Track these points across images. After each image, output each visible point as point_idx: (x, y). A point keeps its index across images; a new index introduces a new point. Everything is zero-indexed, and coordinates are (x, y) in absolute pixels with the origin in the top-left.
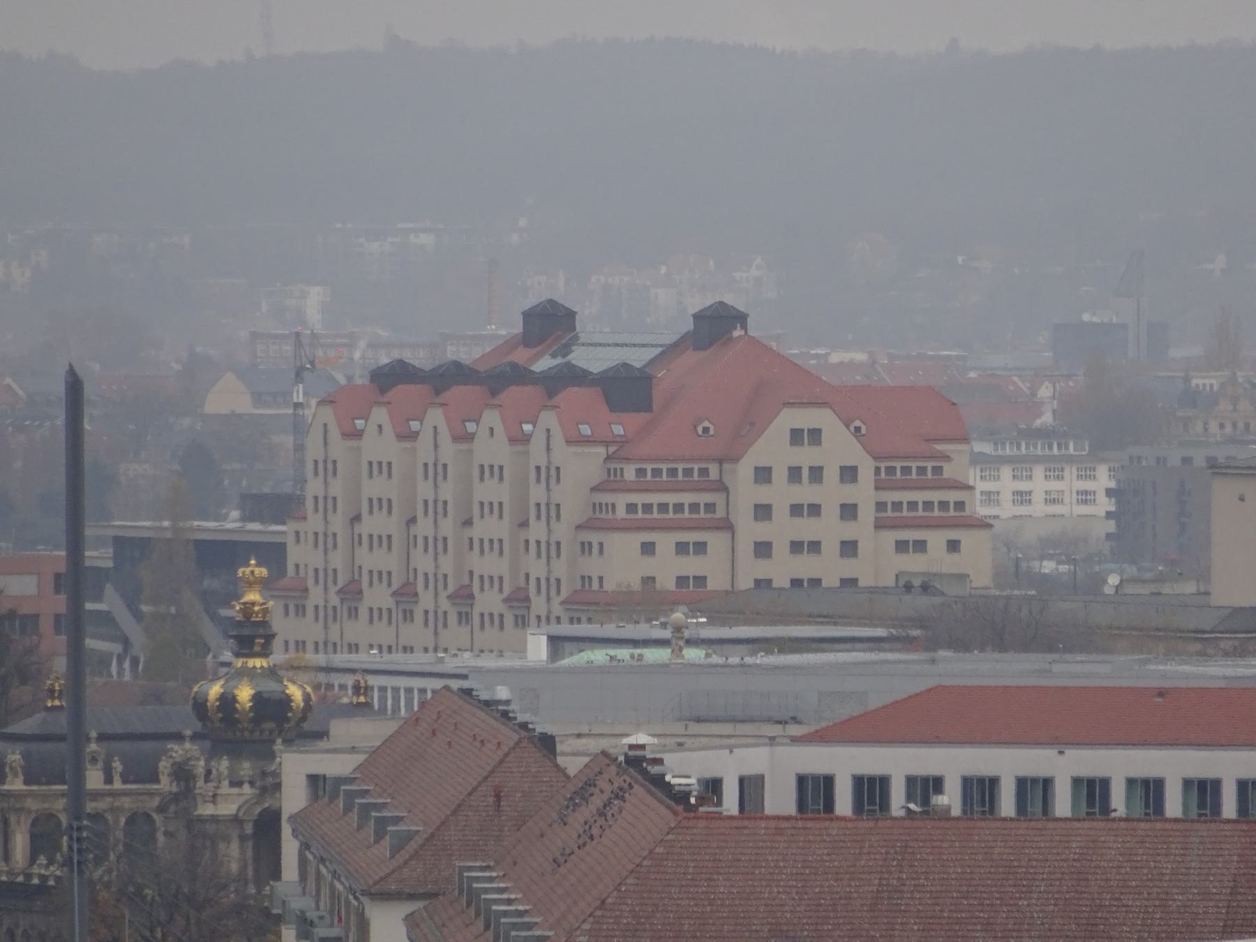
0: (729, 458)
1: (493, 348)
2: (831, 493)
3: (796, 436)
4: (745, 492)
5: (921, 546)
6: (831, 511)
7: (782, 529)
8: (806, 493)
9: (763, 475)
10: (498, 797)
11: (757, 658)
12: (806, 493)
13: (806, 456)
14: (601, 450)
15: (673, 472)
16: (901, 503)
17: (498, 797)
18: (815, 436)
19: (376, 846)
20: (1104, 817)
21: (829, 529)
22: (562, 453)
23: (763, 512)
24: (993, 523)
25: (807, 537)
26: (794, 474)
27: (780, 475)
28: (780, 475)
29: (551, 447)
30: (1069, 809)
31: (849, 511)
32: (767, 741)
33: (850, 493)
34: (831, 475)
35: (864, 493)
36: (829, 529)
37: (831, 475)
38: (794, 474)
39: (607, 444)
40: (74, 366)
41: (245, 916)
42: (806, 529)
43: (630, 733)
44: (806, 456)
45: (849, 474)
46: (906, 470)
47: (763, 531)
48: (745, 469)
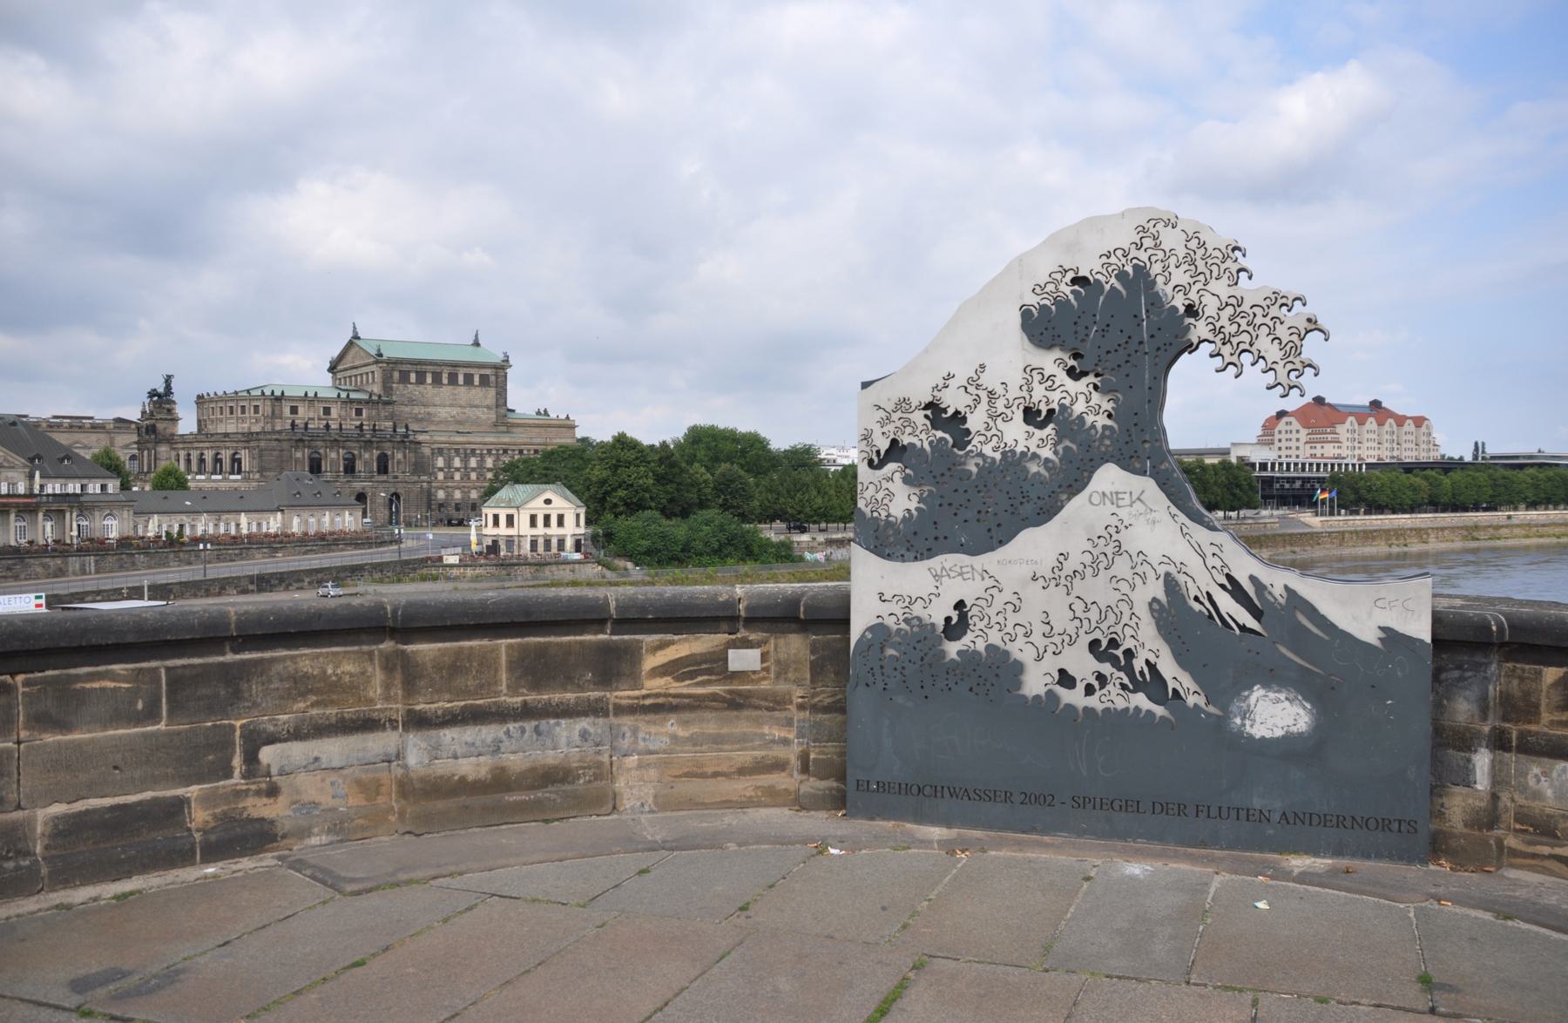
0: (1273, 429)
1: (183, 580)
2: (1294, 436)
4: (1277, 436)
6: (1294, 440)
7: (1284, 444)
8: (1289, 436)
9: (1280, 432)
10: (387, 949)
11: (468, 680)
12: (1289, 436)
13: (1289, 428)
17: (387, 949)
19: (1499, 872)
21: (1293, 444)
23: (1280, 441)
24: (1247, 580)
26: (1287, 432)
27: (1284, 432)
28: (1284, 432)
31: (1298, 440)
34: (1294, 432)
36: (1293, 444)
37: (1294, 432)
38: (1287, 432)
41: (299, 455)
42: (1289, 444)
44: (1289, 428)
45: (1298, 431)
47: (1280, 445)
48: (1276, 431)
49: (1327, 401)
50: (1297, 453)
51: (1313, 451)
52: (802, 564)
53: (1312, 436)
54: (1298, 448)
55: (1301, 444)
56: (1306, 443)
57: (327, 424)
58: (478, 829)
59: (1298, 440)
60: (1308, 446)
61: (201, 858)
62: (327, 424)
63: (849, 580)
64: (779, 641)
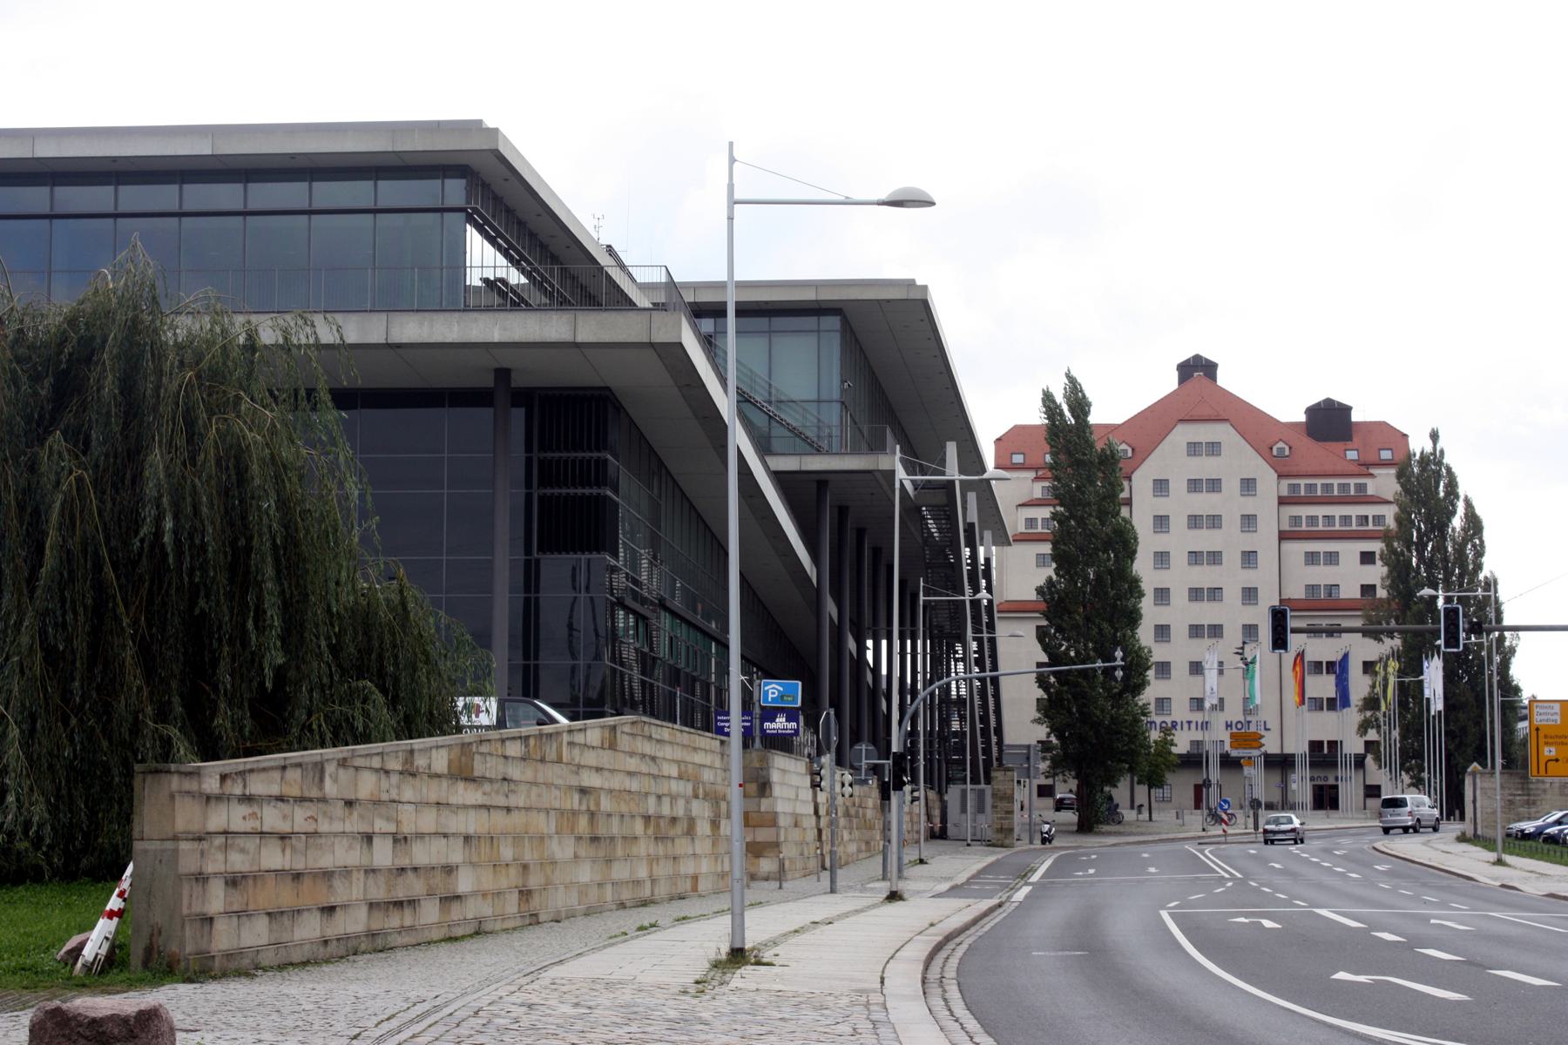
2: (1229, 504)
3: (1194, 449)
5: (1332, 558)
6: (1232, 523)
9: (1161, 486)
13: (1205, 467)
14: (1032, 475)
15: (1343, 487)
16: (1367, 517)
18: (1214, 448)
20: (1492, 588)
21: (1229, 540)
22: (237, 325)
25: (1206, 621)
28: (1178, 486)
29: (1343, 635)
30: (1334, 688)
32: (1401, 831)
33: (1249, 505)
34: (1231, 486)
35: (1265, 504)
36: (1229, 540)
39: (1037, 469)
40: (1474, 504)
43: (1545, 898)
44: (1205, 467)
46: (1327, 487)
49: (1356, 417)
50: (1250, 578)
51: (1321, 575)
52: (740, 386)
53: (1304, 511)
54: (1249, 558)
55: (1265, 539)
56: (1283, 536)
57: (248, 853)
58: (146, 790)
59: (1249, 521)
60: (1297, 549)
61: (1449, 653)
62: (248, 853)
63: (511, 561)
64: (776, 766)
